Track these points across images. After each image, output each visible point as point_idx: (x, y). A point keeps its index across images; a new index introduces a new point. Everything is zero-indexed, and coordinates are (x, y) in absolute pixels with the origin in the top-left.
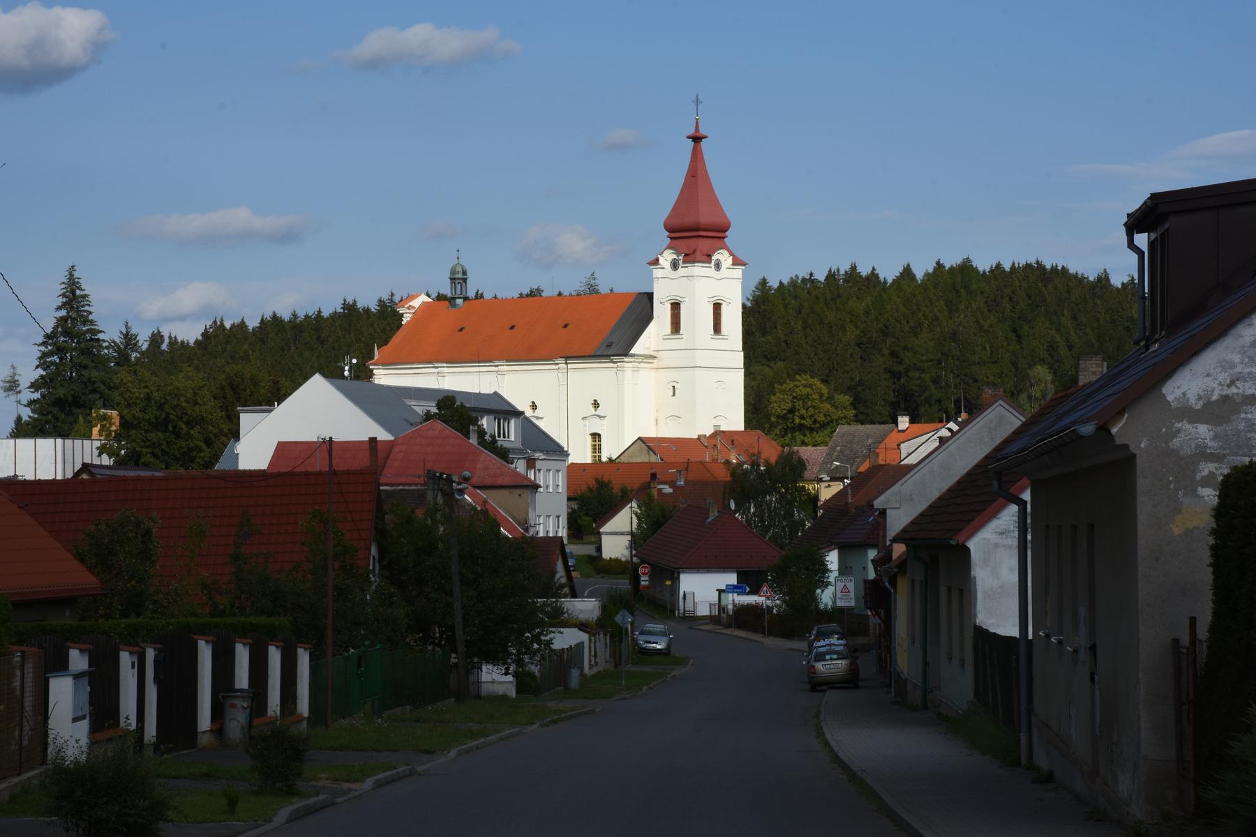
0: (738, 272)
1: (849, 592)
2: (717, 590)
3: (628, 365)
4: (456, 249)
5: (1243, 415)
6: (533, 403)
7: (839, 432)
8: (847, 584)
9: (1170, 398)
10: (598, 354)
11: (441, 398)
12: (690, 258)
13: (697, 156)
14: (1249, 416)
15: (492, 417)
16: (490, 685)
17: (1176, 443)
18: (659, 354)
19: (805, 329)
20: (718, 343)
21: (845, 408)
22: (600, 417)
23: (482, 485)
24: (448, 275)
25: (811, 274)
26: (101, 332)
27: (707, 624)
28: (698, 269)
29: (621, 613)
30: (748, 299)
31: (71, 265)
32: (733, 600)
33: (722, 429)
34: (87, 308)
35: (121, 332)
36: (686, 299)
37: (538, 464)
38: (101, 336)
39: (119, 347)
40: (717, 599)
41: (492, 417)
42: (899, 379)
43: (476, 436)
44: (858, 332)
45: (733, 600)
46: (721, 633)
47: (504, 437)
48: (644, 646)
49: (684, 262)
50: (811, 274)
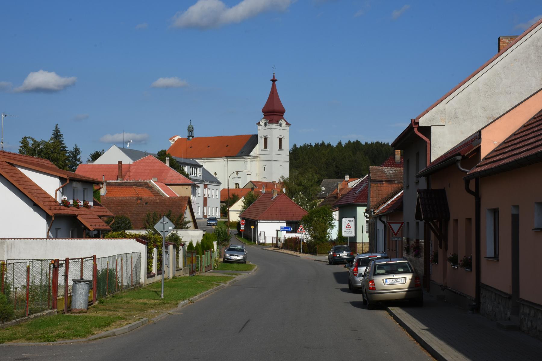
0: (288, 128)
1: (351, 228)
2: (276, 230)
3: (249, 159)
4: (190, 120)
6: (215, 173)
7: (324, 182)
8: (349, 223)
10: (238, 155)
11: (160, 151)
12: (271, 122)
13: (274, 87)
15: (190, 167)
18: (260, 156)
19: (308, 159)
20: (280, 152)
21: (324, 176)
22: (238, 177)
23: (170, 184)
24: (187, 129)
25: (310, 144)
26: (66, 147)
27: (271, 247)
28: (274, 126)
29: (161, 221)
30: (291, 150)
31: (56, 124)
32: (284, 236)
34: (62, 139)
35: (74, 148)
36: (269, 136)
37: (209, 187)
38: (66, 149)
39: (73, 153)
40: (276, 235)
41: (190, 167)
42: (338, 174)
43: (169, 162)
44: (325, 160)
45: (284, 236)
46: (278, 252)
47: (195, 175)
48: (230, 258)
49: (269, 123)
50: (310, 144)
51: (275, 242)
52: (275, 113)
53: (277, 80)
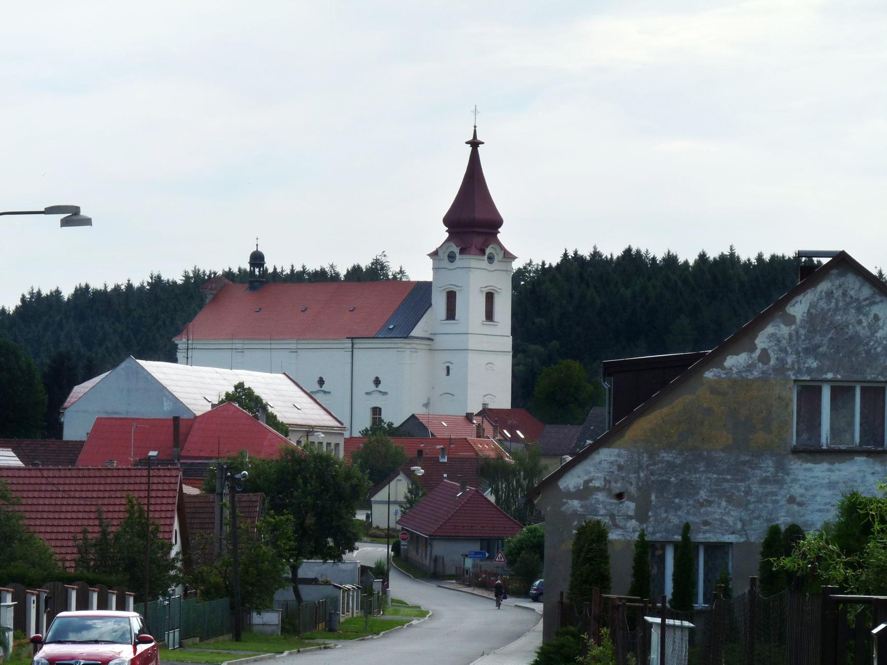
5: (594, 496)
9: (561, 487)
14: (597, 496)
16: (261, 626)
17: (563, 508)
20: (489, 329)
33: (491, 406)
51: (348, 343)
52: (476, 230)
53: (483, 143)
